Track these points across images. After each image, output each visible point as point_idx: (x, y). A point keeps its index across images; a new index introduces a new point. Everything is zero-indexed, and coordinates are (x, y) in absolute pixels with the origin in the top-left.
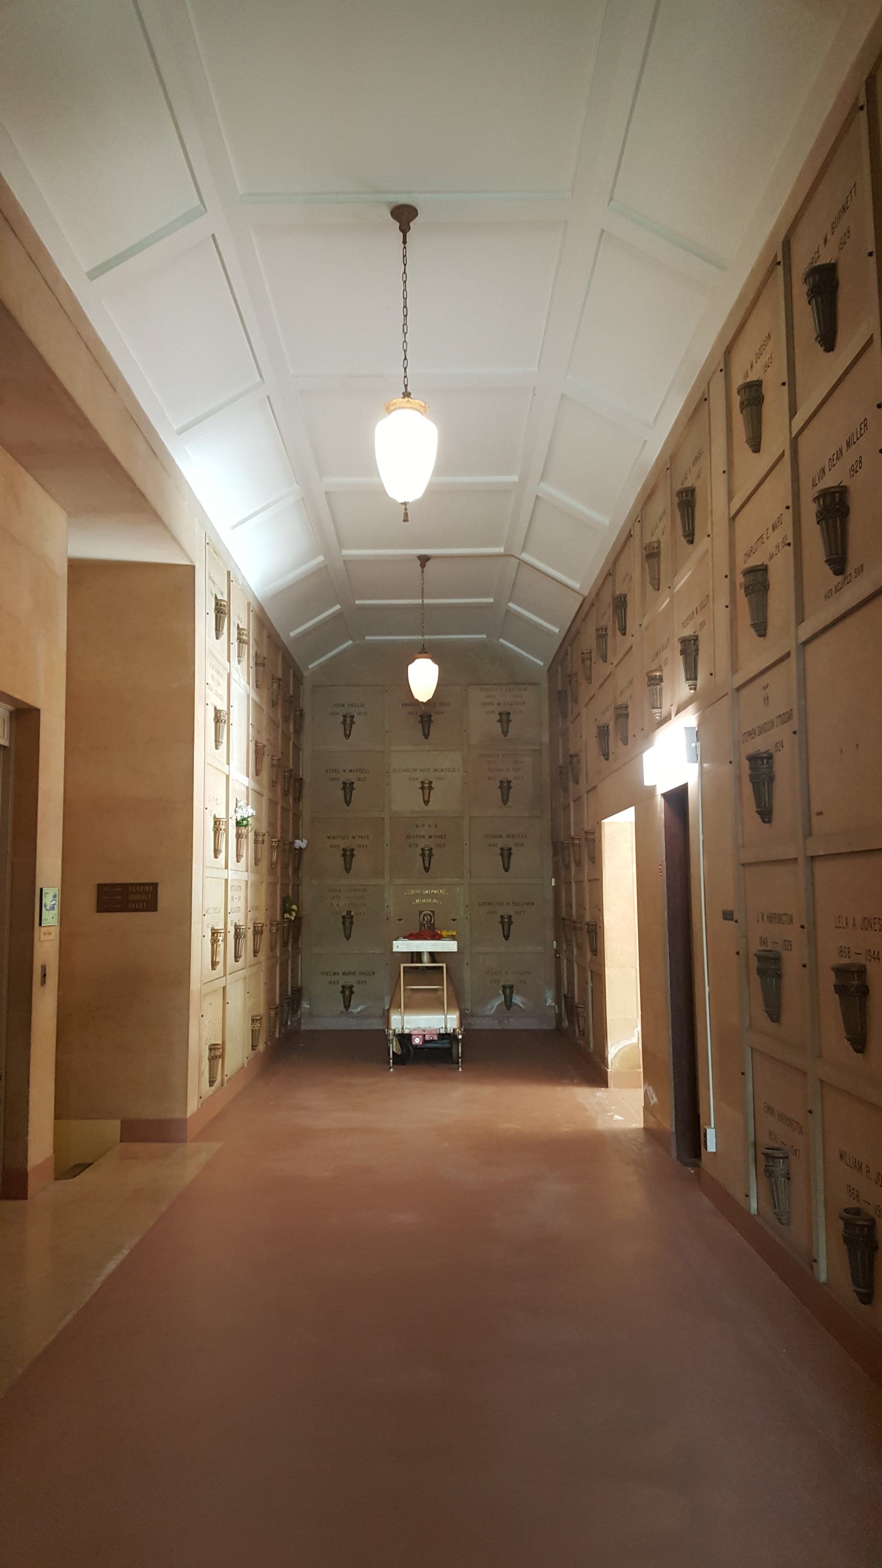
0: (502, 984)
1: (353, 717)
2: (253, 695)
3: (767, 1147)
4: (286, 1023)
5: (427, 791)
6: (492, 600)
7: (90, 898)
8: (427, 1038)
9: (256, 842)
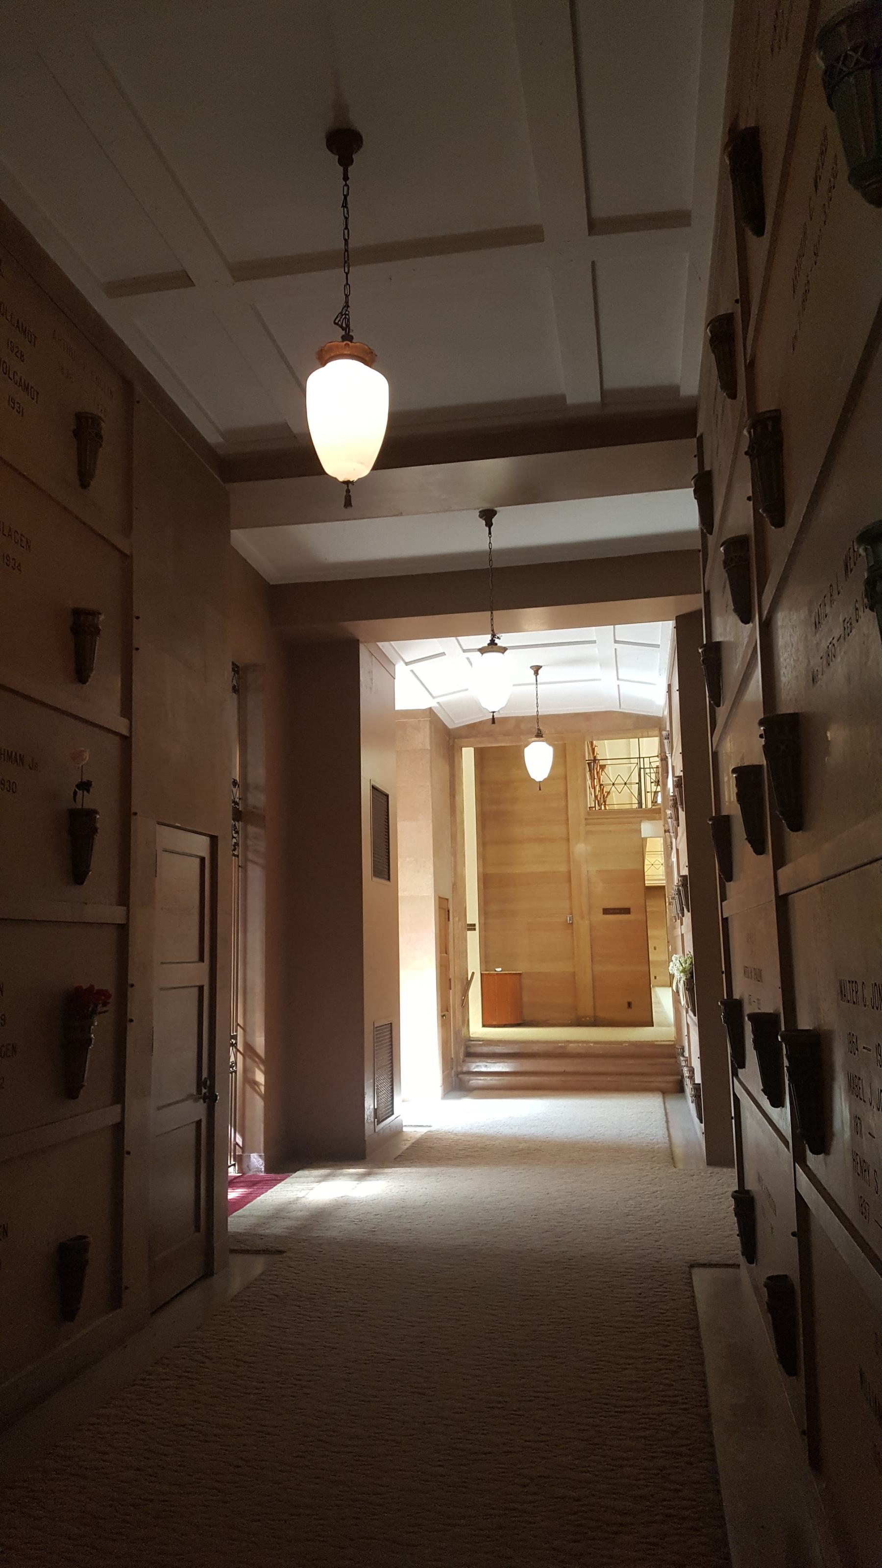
3: (447, 920)
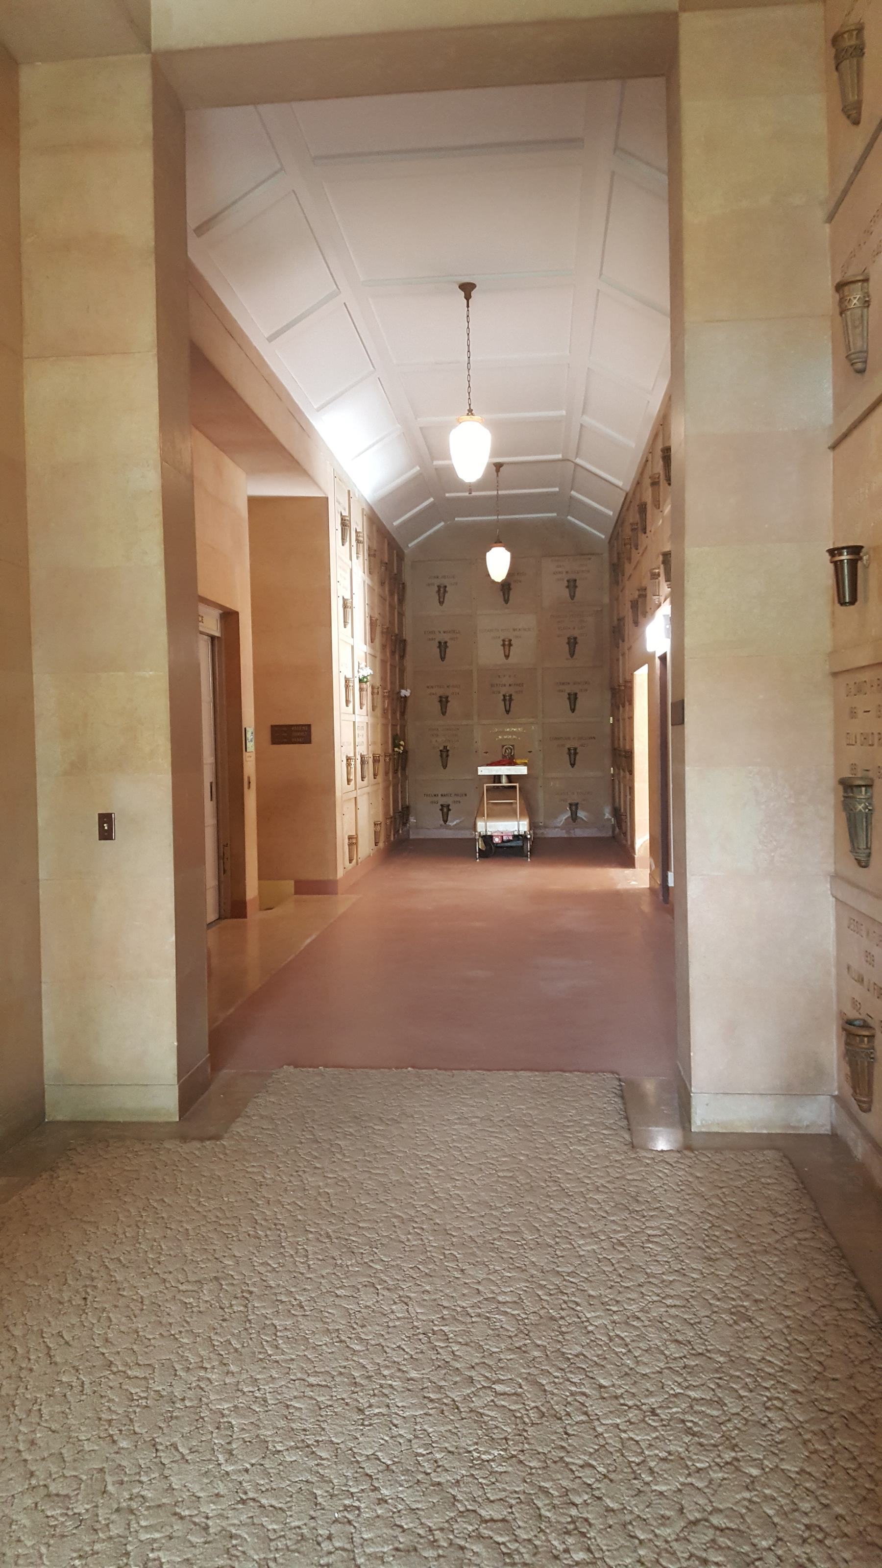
0: (569, 802)
1: (446, 587)
2: (368, 581)
4: (399, 831)
5: (507, 647)
6: (557, 489)
7: (267, 735)
8: (505, 838)
9: (373, 693)
